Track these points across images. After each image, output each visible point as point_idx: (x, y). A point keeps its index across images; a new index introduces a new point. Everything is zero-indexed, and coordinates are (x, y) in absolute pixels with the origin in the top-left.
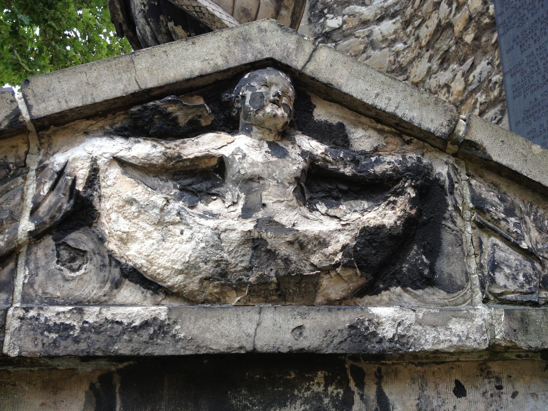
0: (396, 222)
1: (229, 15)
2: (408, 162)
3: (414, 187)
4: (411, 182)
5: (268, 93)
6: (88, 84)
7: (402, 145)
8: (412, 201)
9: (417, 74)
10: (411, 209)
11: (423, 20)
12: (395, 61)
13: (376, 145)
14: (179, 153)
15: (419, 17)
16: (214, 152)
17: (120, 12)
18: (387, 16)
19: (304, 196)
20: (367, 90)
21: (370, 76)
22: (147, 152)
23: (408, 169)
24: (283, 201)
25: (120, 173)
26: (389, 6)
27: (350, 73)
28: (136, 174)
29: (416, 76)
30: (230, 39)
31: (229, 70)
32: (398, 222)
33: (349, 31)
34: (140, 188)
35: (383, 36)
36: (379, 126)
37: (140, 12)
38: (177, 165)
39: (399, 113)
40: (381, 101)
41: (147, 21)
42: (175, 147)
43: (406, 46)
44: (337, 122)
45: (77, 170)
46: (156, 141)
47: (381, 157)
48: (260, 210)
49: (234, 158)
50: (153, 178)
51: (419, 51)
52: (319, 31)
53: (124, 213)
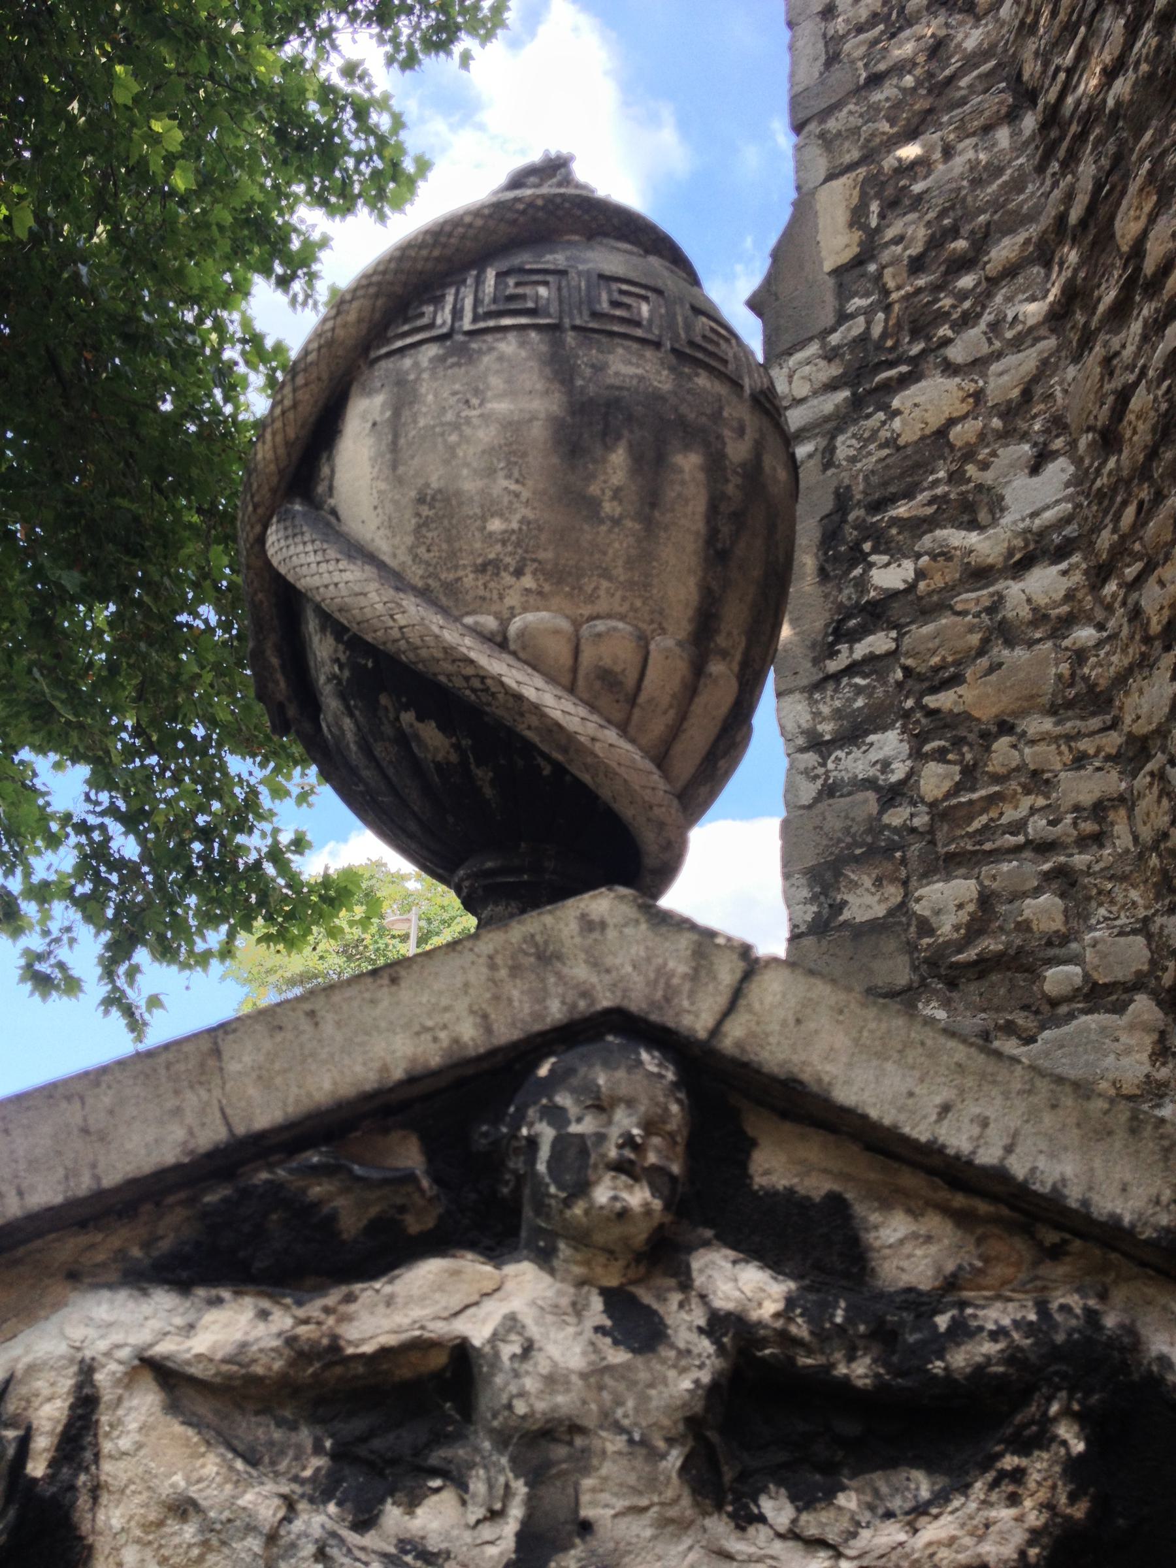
0: (1023, 1554)
1: (559, 692)
2: (1055, 1326)
3: (1082, 1419)
4: (1071, 1398)
5: (601, 1138)
6: (85, 1131)
7: (1036, 1264)
8: (1074, 1468)
9: (1144, 710)
10: (1073, 1498)
11: (1147, 565)
12: (1073, 675)
13: (950, 1267)
14: (335, 1338)
15: (1137, 557)
16: (439, 1329)
17: (279, 676)
18: (1044, 552)
19: (719, 1474)
20: (911, 1094)
21: (920, 1050)
22: (238, 1336)
23: (1056, 1353)
24: (645, 1509)
25: (157, 1409)
26: (1047, 527)
27: (856, 1041)
28: (204, 1408)
29: (1139, 717)
30: (499, 960)
31: (493, 1053)
32: (1033, 1552)
33: (935, 598)
34: (211, 1465)
35: (1035, 610)
36: (959, 1200)
37: (329, 680)
38: (327, 1374)
39: (1018, 1168)
40: (959, 1129)
41: (347, 706)
42: (322, 1316)
43: (1105, 634)
44: (823, 1192)
45: (36, 1403)
46: (270, 1296)
47: (969, 1311)
48: (573, 1546)
49: (497, 1355)
50: (253, 1419)
51: (1143, 648)
52: (850, 598)
53: (161, 1546)
